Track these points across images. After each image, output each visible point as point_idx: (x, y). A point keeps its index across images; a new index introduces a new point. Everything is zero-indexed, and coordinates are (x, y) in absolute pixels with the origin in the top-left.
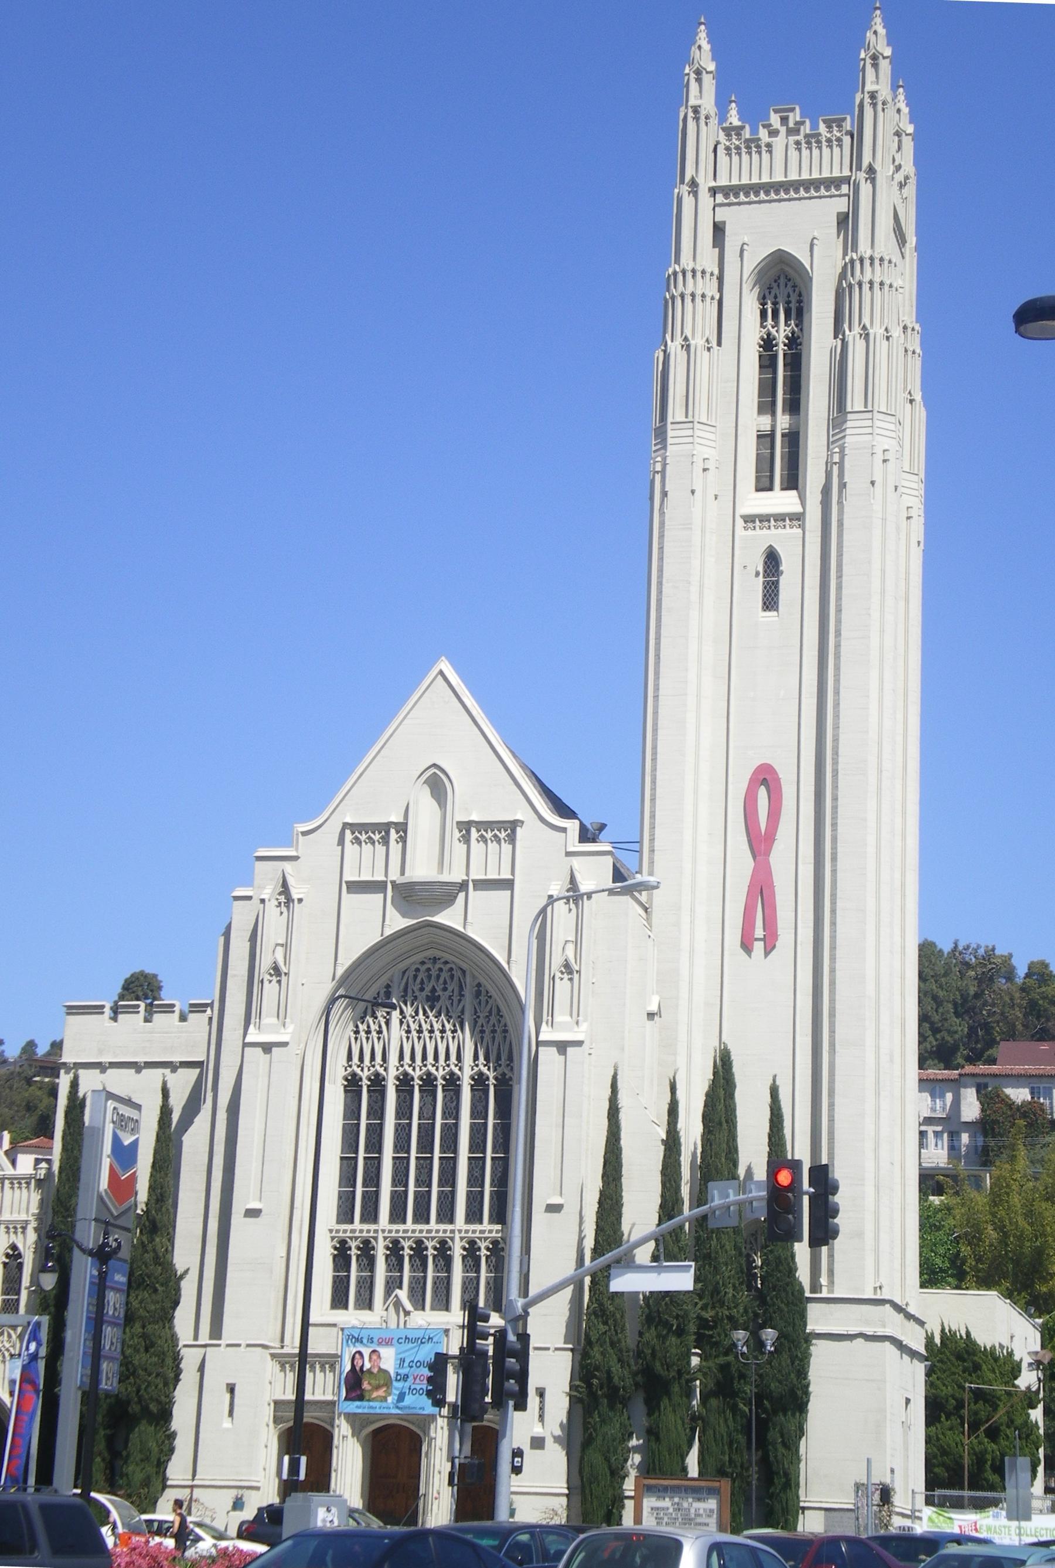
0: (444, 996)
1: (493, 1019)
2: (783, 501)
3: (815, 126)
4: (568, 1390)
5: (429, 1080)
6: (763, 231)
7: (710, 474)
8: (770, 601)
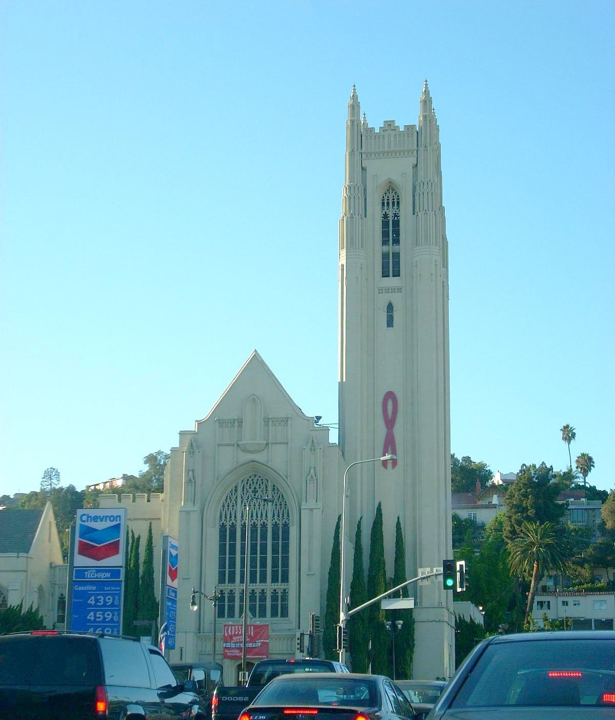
8: (390, 323)
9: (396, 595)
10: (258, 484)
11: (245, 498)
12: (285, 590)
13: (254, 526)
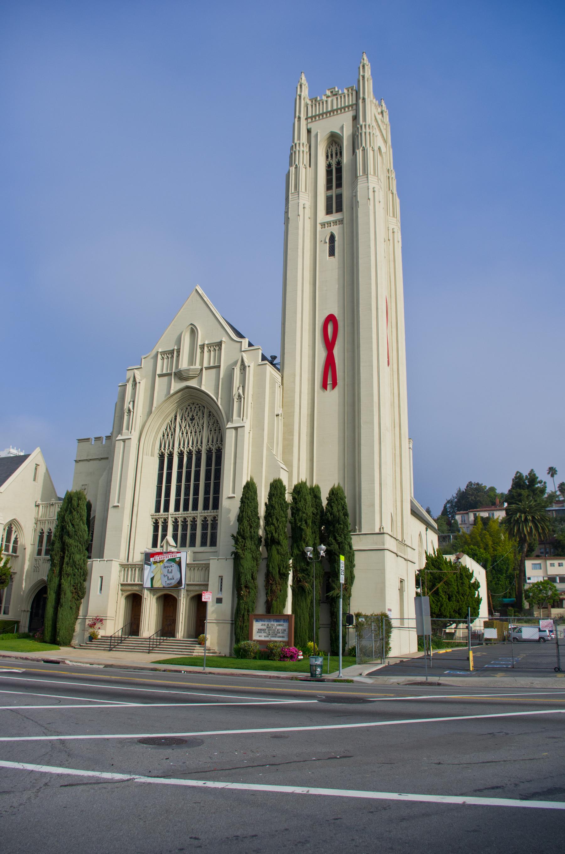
0: (196, 418)
2: (335, 217)
3: (343, 90)
7: (280, 417)
10: (196, 412)
11: (184, 425)
12: (215, 518)
13: (190, 453)
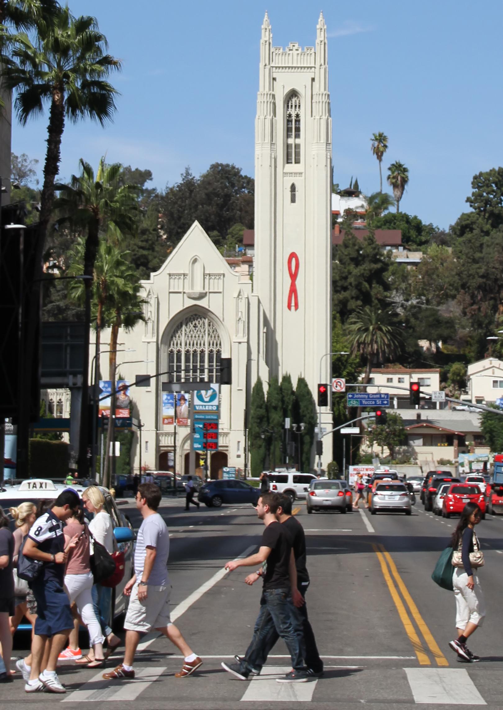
1: (215, 332)
4: (268, 381)
5: (195, 351)
6: (286, 82)
8: (293, 200)
9: (349, 426)
